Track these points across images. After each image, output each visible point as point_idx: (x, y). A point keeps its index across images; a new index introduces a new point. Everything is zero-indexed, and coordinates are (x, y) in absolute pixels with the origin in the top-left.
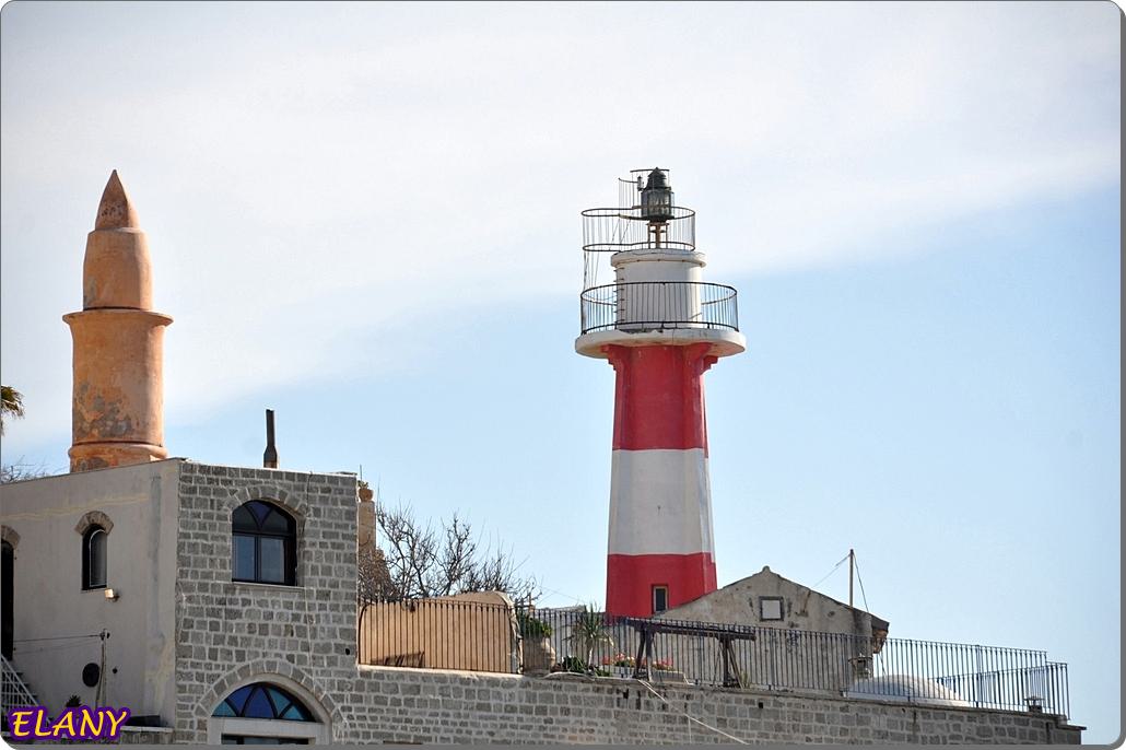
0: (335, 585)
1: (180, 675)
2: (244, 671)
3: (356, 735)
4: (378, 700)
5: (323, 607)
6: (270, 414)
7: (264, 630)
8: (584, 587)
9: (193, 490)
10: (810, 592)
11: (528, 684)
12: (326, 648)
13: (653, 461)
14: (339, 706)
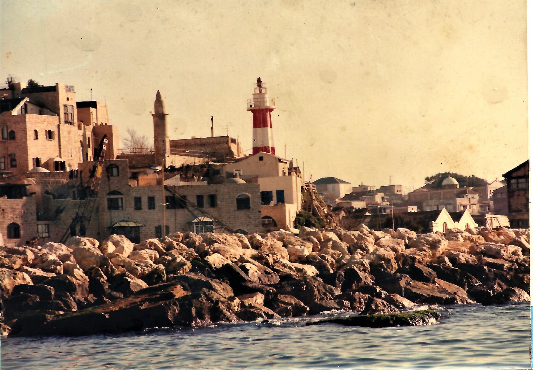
13: (259, 130)
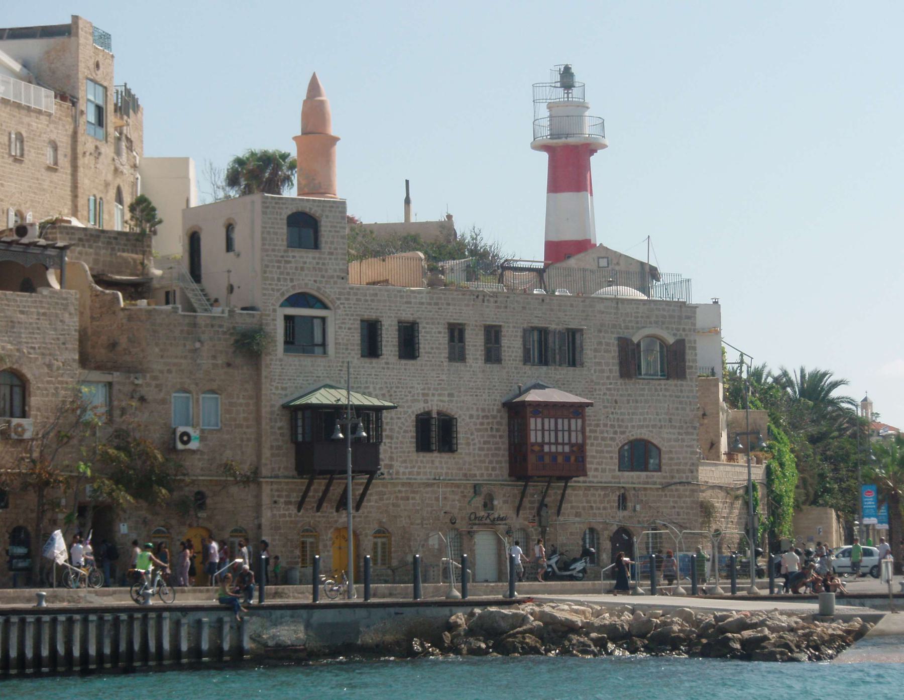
0: (336, 249)
1: (264, 289)
2: (293, 287)
3: (347, 315)
4: (358, 300)
5: (330, 259)
6: (407, 182)
7: (302, 269)
8: (533, 253)
9: (267, 207)
10: (621, 255)
11: (430, 293)
12: (332, 277)
13: (566, 198)
14: (338, 302)
